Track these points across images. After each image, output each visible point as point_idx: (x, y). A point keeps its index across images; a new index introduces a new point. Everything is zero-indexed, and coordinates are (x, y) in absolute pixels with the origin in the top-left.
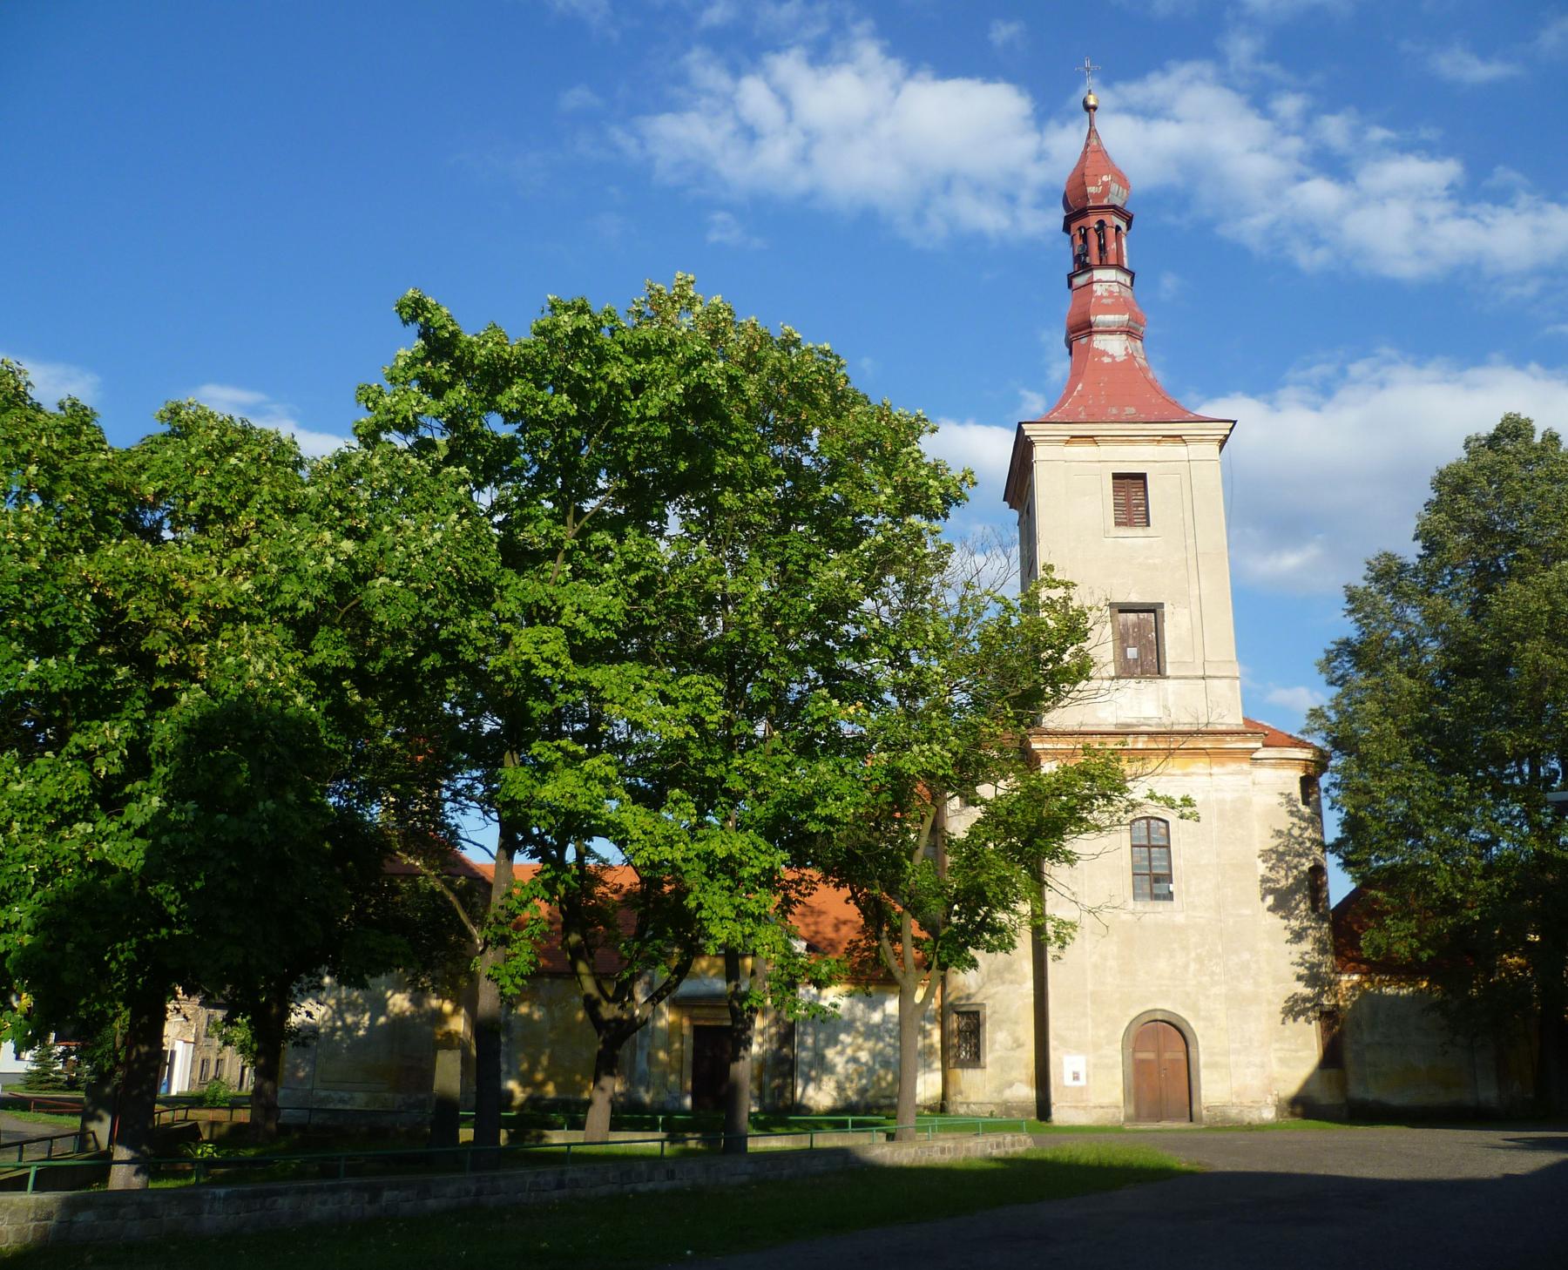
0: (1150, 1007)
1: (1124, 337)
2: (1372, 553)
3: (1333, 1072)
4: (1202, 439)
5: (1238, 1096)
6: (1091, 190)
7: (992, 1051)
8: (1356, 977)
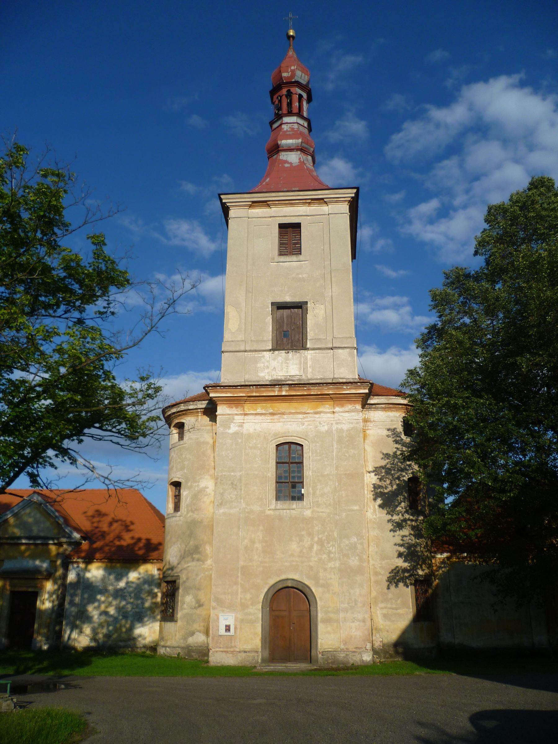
0: (283, 577)
1: (299, 152)
4: (337, 201)
5: (345, 644)
6: (285, 75)
8: (445, 555)
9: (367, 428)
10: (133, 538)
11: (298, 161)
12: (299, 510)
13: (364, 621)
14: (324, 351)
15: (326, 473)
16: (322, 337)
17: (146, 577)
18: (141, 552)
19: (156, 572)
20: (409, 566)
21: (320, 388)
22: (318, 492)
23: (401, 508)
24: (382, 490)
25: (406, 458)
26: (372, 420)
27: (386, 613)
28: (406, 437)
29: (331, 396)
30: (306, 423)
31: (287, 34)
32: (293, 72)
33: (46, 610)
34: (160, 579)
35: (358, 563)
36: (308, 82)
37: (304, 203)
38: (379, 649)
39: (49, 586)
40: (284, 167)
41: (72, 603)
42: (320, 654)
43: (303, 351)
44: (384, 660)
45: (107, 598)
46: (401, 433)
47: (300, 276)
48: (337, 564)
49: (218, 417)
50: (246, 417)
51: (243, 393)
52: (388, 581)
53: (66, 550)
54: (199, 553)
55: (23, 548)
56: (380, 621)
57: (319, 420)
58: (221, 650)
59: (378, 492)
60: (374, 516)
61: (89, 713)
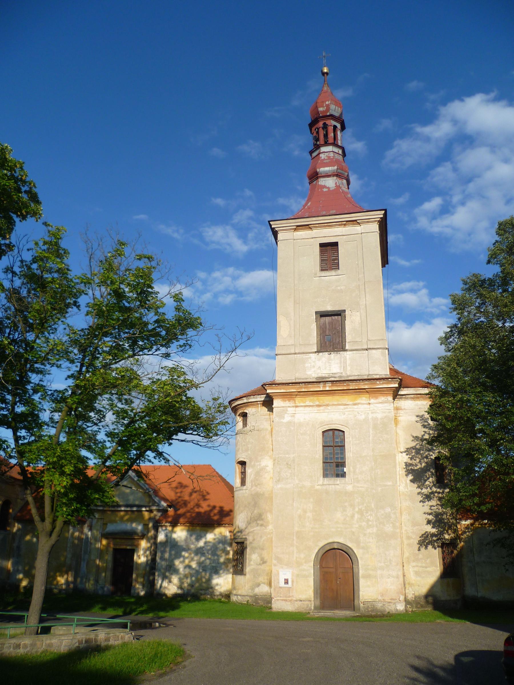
0: (331, 540)
1: (335, 178)
2: (466, 274)
3: (450, 580)
5: (382, 595)
6: (321, 109)
7: (249, 565)
8: (468, 522)
9: (398, 415)
10: (209, 506)
11: (334, 185)
12: (342, 485)
13: (398, 577)
14: (360, 352)
15: (364, 455)
16: (358, 339)
17: (220, 538)
18: (216, 518)
19: (228, 534)
20: (437, 532)
21: (357, 383)
22: (357, 470)
23: (429, 483)
24: (413, 468)
25: (431, 442)
26: (403, 408)
27: (417, 570)
28: (432, 422)
29: (367, 390)
30: (347, 413)
31: (322, 71)
32: (328, 106)
33: (141, 564)
34: (231, 539)
35: (392, 529)
36: (341, 114)
37: (340, 225)
38: (411, 600)
39: (144, 544)
40: (323, 191)
41: (162, 558)
42: (361, 603)
43: (343, 352)
44: (416, 609)
45: (190, 554)
46: (428, 418)
47: (339, 288)
48: (375, 530)
49: (274, 409)
50: (297, 408)
51: (294, 389)
52: (418, 544)
53: (155, 515)
54: (262, 520)
55: (122, 513)
56: (412, 577)
57: (357, 410)
58: (282, 598)
59: (409, 470)
60: (406, 490)
61: (185, 644)
